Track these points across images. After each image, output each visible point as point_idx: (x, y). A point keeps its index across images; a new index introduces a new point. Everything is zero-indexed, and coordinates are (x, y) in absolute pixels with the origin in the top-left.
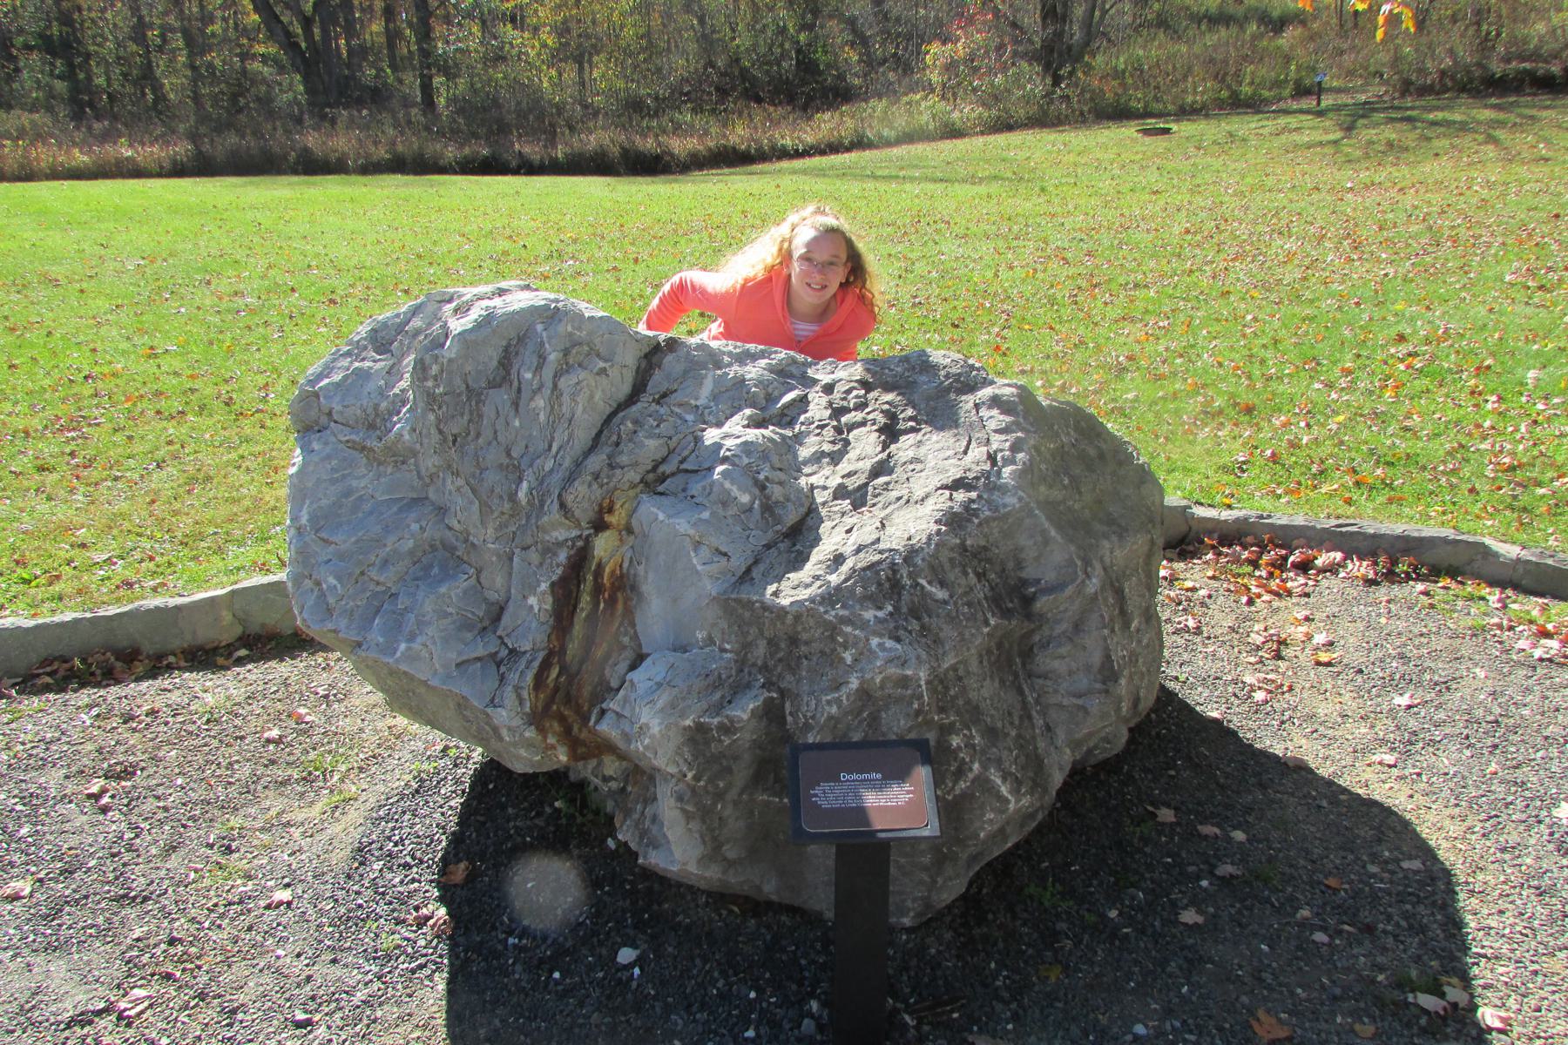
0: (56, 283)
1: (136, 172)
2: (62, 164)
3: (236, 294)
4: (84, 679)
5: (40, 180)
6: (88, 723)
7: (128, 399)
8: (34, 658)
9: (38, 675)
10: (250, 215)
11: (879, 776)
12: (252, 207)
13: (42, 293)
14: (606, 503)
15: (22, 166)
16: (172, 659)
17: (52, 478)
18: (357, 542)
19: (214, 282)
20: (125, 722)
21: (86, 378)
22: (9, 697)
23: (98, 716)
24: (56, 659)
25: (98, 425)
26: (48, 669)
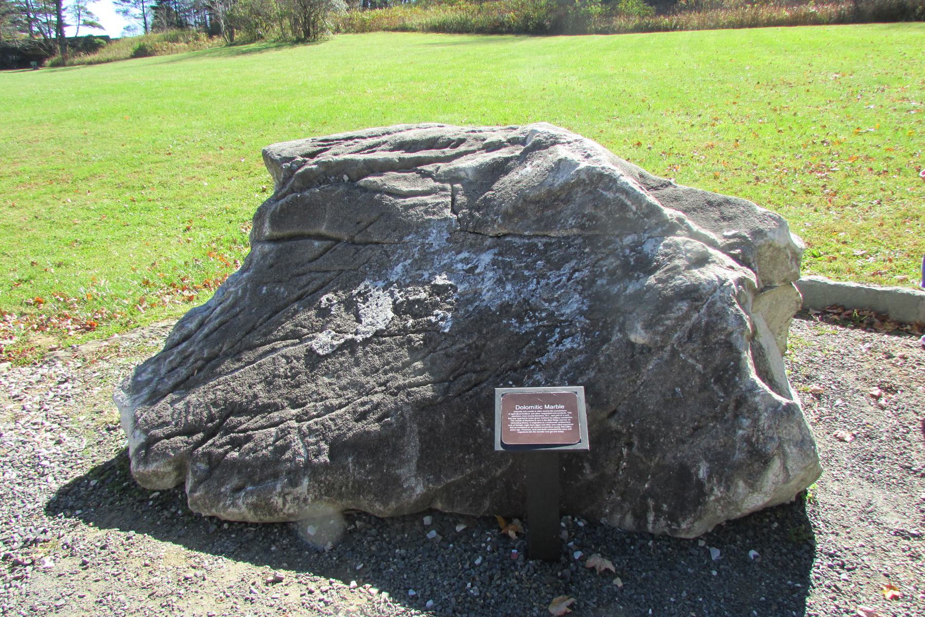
0: (790, 85)
1: (816, 21)
2: (774, 18)
3: (903, 99)
4: (857, 323)
5: (760, 26)
6: (864, 351)
7: (850, 159)
8: (828, 302)
9: (829, 313)
10: (897, 47)
11: (563, 407)
12: (897, 43)
13: (785, 90)
14: (729, 211)
15: (753, 19)
16: (909, 327)
17: (815, 199)
18: (679, 219)
19: (887, 90)
20: (887, 358)
21: (823, 142)
22: (815, 321)
23: (870, 348)
24: (840, 306)
25: (834, 171)
26: (835, 311)
